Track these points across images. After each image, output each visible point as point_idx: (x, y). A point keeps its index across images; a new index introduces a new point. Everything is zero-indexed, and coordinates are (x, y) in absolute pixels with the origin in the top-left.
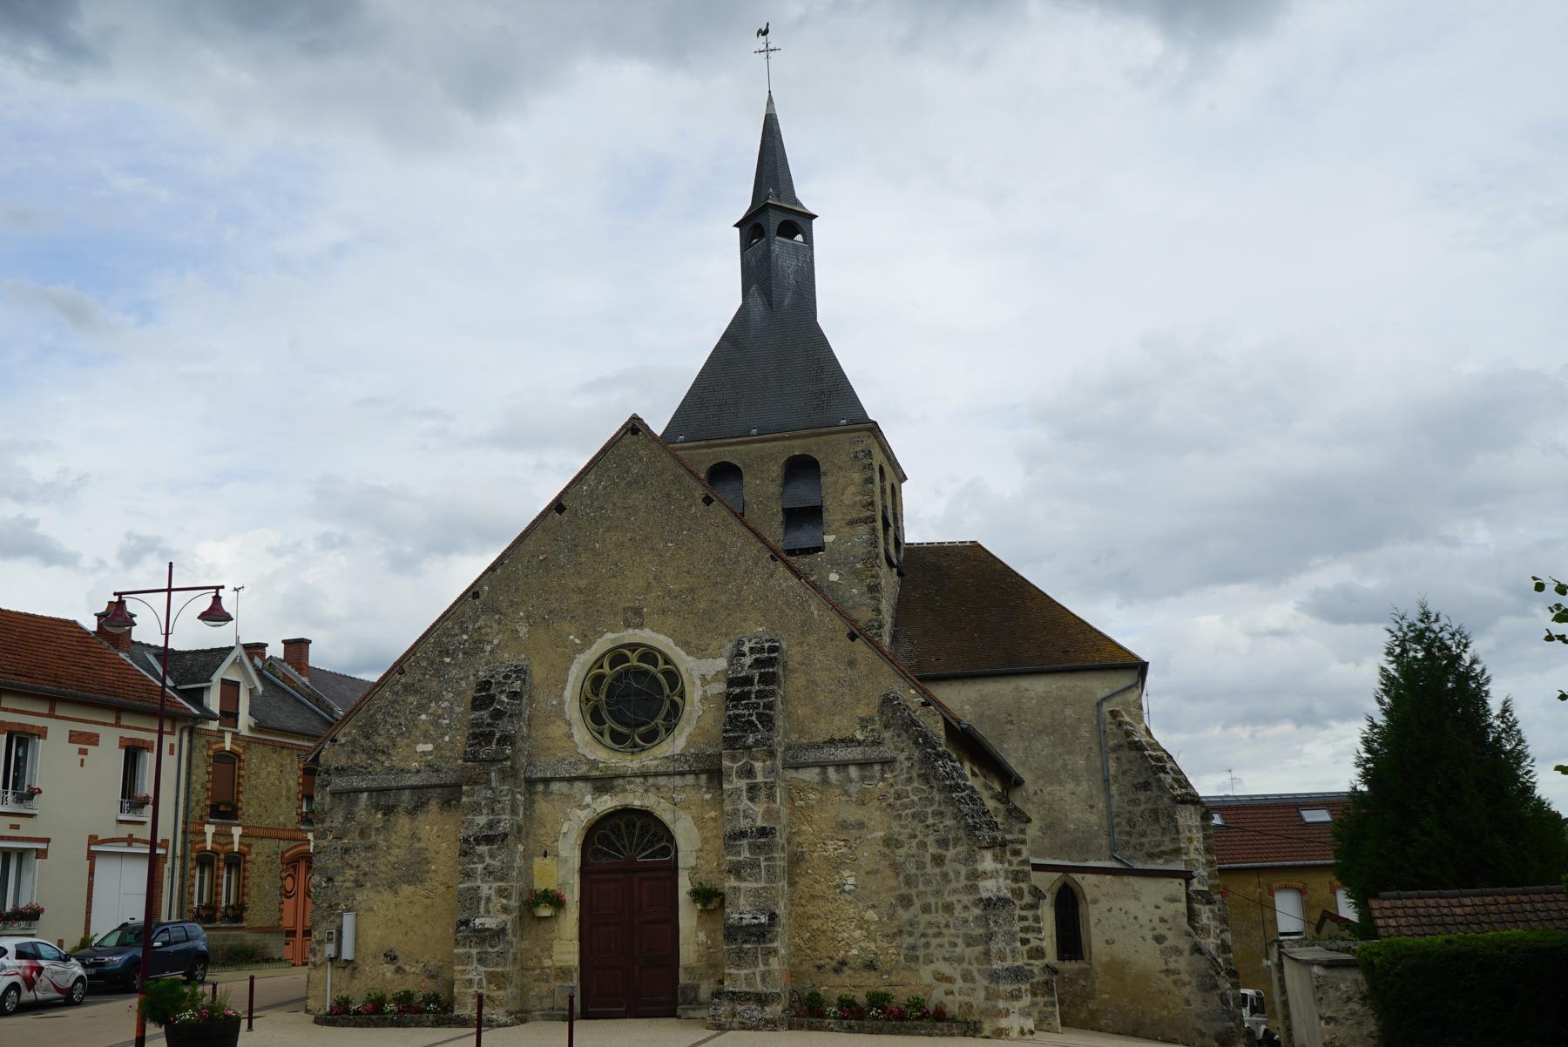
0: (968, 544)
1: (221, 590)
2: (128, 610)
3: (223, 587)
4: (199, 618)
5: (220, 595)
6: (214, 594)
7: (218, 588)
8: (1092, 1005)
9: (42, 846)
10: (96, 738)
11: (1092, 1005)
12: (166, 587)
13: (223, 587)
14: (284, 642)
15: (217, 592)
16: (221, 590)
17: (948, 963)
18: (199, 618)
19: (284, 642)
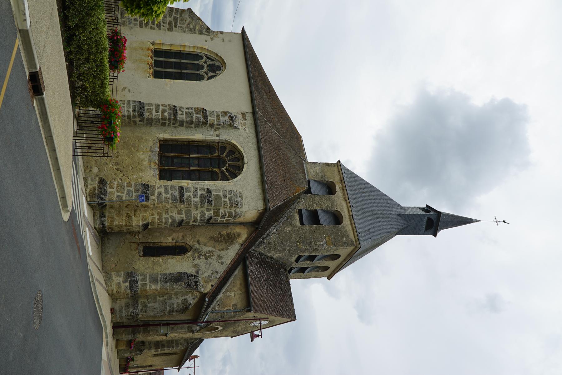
0: (303, 143)
1: (261, 337)
2: (207, 343)
3: (262, 337)
4: (436, 237)
5: (259, 337)
6: (259, 335)
7: (261, 336)
8: (238, 210)
9: (116, 78)
10: (294, 319)
11: (238, 210)
12: (262, 330)
13: (262, 337)
14: (427, 205)
15: (260, 336)
16: (261, 337)
17: (212, 111)
18: (436, 237)
19: (427, 205)
